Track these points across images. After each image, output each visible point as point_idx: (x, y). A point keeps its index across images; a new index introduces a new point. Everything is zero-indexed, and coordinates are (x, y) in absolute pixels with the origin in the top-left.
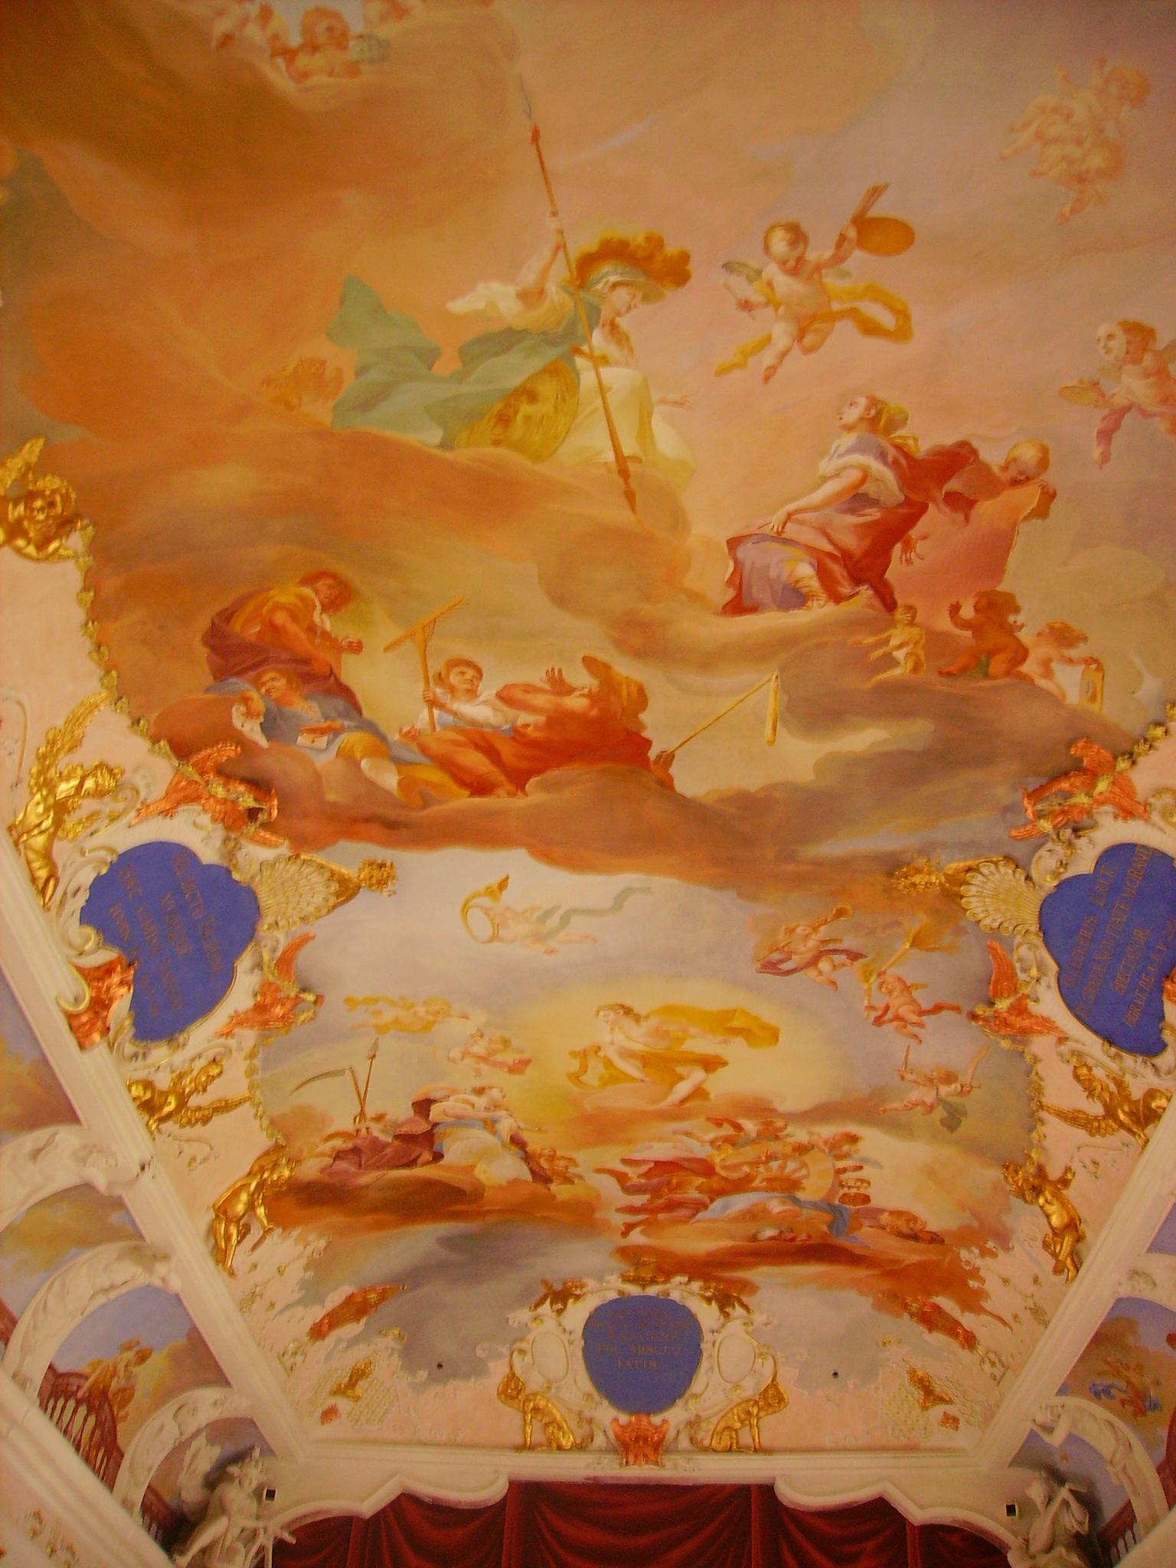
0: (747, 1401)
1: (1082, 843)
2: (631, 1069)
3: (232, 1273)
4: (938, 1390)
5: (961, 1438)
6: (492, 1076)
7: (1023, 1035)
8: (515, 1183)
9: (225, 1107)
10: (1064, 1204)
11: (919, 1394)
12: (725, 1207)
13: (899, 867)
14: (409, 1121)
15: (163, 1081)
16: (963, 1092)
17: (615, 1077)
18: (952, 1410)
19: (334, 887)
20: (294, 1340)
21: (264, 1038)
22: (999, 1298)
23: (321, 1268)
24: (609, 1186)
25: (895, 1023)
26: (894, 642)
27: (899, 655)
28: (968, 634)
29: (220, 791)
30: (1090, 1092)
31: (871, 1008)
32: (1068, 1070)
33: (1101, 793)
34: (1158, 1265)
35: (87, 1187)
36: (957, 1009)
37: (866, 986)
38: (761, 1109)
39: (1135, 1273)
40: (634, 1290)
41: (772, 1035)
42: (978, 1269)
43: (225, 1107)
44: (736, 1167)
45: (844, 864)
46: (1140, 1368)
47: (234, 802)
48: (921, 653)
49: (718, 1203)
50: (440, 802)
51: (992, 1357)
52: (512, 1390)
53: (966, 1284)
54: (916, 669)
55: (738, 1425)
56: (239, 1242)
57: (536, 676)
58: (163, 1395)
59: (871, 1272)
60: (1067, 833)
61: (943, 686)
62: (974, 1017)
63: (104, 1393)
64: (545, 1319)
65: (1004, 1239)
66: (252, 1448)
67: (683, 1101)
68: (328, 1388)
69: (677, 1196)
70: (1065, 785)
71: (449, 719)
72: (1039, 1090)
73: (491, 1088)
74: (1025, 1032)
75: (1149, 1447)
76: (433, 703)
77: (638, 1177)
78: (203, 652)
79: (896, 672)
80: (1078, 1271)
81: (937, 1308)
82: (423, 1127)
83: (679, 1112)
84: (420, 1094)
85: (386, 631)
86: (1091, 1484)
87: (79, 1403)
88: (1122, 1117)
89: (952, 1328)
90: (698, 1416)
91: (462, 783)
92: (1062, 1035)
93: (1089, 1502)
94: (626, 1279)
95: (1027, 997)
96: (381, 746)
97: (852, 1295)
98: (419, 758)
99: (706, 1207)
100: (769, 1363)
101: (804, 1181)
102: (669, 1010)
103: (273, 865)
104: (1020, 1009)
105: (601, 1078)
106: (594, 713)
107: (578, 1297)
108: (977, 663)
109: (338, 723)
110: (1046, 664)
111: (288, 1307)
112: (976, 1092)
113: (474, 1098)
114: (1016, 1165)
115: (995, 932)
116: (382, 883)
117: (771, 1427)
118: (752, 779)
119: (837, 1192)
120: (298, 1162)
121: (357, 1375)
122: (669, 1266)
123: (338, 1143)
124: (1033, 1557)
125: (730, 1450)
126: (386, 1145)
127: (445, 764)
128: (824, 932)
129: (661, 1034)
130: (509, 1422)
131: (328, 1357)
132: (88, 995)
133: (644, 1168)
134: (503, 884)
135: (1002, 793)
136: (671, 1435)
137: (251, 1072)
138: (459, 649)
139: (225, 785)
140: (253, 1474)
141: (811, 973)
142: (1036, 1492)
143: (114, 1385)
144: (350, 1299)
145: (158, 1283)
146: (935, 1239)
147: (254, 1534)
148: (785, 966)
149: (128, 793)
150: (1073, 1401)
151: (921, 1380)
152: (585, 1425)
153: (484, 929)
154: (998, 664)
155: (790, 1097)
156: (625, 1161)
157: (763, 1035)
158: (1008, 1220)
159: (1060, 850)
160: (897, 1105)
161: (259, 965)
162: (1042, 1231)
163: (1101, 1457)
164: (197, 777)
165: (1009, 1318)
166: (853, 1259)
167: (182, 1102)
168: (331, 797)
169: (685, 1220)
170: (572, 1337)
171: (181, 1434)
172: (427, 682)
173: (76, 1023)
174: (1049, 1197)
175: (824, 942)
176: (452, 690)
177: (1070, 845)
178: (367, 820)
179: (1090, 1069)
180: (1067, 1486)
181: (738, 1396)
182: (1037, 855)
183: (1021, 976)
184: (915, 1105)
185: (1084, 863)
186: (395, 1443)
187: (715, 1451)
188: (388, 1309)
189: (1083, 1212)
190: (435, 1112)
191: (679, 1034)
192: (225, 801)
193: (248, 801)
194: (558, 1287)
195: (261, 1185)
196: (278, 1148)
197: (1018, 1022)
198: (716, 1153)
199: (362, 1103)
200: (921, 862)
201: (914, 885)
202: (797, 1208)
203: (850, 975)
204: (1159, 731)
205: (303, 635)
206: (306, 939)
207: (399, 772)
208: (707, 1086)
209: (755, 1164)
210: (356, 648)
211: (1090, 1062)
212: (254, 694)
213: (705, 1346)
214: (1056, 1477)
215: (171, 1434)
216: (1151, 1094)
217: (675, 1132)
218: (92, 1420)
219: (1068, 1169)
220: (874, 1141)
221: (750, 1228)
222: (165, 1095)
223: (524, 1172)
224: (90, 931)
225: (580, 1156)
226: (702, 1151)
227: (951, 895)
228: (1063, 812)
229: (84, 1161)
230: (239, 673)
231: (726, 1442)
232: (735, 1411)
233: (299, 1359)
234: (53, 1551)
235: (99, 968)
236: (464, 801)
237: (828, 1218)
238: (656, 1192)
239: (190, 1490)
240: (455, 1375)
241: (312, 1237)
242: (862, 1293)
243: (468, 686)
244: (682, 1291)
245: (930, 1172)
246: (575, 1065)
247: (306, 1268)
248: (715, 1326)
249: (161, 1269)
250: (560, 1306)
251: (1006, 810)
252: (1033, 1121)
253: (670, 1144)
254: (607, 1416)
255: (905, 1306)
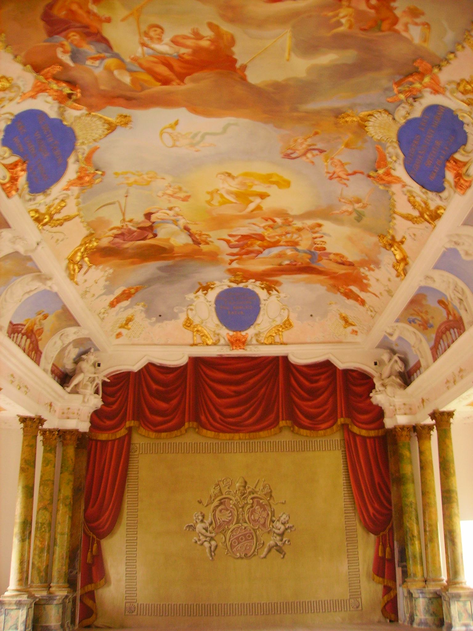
0: (278, 326)
1: (416, 104)
2: (231, 198)
3: (77, 284)
4: (350, 321)
5: (358, 338)
6: (176, 203)
7: (388, 184)
8: (186, 245)
9: (68, 219)
10: (401, 250)
11: (343, 323)
12: (269, 253)
13: (340, 114)
14: (143, 222)
15: (43, 210)
16: (364, 207)
17: (225, 202)
18: (355, 328)
19: (106, 126)
20: (103, 308)
21: (82, 190)
22: (375, 287)
23: (112, 281)
24: (223, 246)
25: (337, 179)
26: (341, 15)
27: (343, 21)
28: (373, 11)
29: (55, 86)
30: (414, 206)
31: (328, 173)
32: (405, 198)
33: (425, 83)
34: (437, 275)
35: (17, 253)
36: (362, 173)
37: (326, 164)
38: (283, 214)
39: (427, 277)
40: (234, 285)
41: (287, 184)
42: (367, 276)
43: (68, 219)
44: (274, 237)
45: (318, 113)
46: (427, 313)
47: (61, 91)
48: (352, 20)
49: (266, 251)
50: (150, 88)
51: (372, 309)
52: (188, 324)
53: (362, 281)
54: (350, 27)
55: (274, 335)
56: (79, 271)
57: (187, 32)
58: (54, 331)
59: (326, 277)
60: (411, 100)
61: (361, 35)
62: (369, 176)
63: (32, 331)
64: (200, 297)
65: (377, 264)
66: (90, 349)
67: (252, 211)
68: (118, 325)
69: (250, 249)
70: (411, 79)
71: (151, 51)
72: (394, 206)
73: (175, 207)
74: (389, 183)
75: (428, 340)
76: (143, 45)
77: (236, 241)
78: (42, 24)
79: (341, 29)
80: (405, 276)
81: (351, 291)
82: (148, 224)
83: (251, 216)
84: (147, 210)
85: (121, 12)
86: (405, 354)
87: (23, 335)
88: (426, 217)
89: (356, 298)
90: (259, 332)
91: (158, 80)
92: (403, 184)
93: (405, 361)
94: (231, 281)
95: (391, 168)
96: (122, 65)
97: (318, 286)
98: (139, 69)
99: (261, 252)
100: (286, 312)
101: (300, 242)
102: (246, 174)
103: (79, 118)
104: (388, 174)
105: (219, 202)
106: (213, 48)
107: (212, 288)
108: (377, 25)
109: (103, 55)
110: (406, 25)
111: (101, 295)
112: (369, 207)
113: (168, 212)
114: (383, 235)
115: (379, 142)
116: (126, 124)
117: (286, 335)
118: (280, 76)
119: (313, 246)
120: (100, 239)
121: (129, 320)
122: (247, 276)
123: (115, 232)
124: (383, 380)
125: (271, 344)
126: (134, 232)
127: (150, 72)
128: (309, 141)
129: (243, 184)
130: (188, 336)
131: (117, 314)
132: (8, 175)
133: (237, 238)
134: (176, 123)
135: (385, 83)
136: (249, 338)
137: (78, 204)
138: (154, 20)
139: (57, 84)
140: (92, 358)
141: (304, 158)
142: (385, 357)
143: (36, 328)
144: (124, 293)
145: (48, 289)
146: (351, 264)
147: (94, 380)
148: (293, 156)
149: (15, 89)
150: (400, 325)
151: (344, 317)
152: (216, 336)
153: (170, 142)
154: (385, 25)
155: (295, 210)
156: (230, 236)
157: (284, 184)
158: (380, 257)
159: (407, 107)
160: (337, 212)
161: (77, 161)
162: (392, 260)
163: (409, 344)
164: (44, 81)
165: (378, 294)
166: (319, 272)
167: (51, 218)
168: (102, 87)
169: (253, 258)
170: (210, 303)
171: (64, 344)
172: (140, 36)
173: (5, 187)
174: (396, 248)
175: (310, 145)
176: (151, 38)
177: (411, 105)
178: (118, 97)
179: (414, 197)
180: (397, 355)
181: (275, 324)
182: (397, 109)
183: (389, 160)
184: (345, 212)
185: (417, 112)
186: (144, 345)
187: (266, 344)
188: (139, 295)
189: (409, 253)
190: (153, 218)
191: (250, 184)
192: (57, 91)
193: (67, 90)
194: (204, 285)
195: (86, 249)
196: (91, 234)
197: (387, 178)
198: (265, 231)
199: (124, 214)
200: (349, 112)
201: (347, 122)
202: (297, 252)
203: (319, 159)
204: (452, 56)
205: (85, 15)
206: (97, 149)
207: (131, 76)
208: (262, 205)
209: (280, 236)
210: (109, 20)
211: (415, 195)
212: (65, 43)
213: (261, 306)
214: (393, 352)
215: (59, 345)
216: (438, 208)
217: (250, 223)
218: (29, 341)
219: (404, 237)
220: (328, 226)
221: (279, 261)
222: (44, 215)
223: (189, 240)
224: (6, 149)
225: (211, 233)
226: (260, 231)
227: (362, 126)
228: (410, 91)
229: (14, 243)
230: (58, 33)
231: (270, 341)
232: (273, 329)
233: (106, 315)
234: (20, 388)
235: (11, 164)
236: (158, 88)
237: (309, 256)
238: (242, 247)
239: (69, 365)
240: (166, 319)
241: (107, 268)
242: (323, 285)
243: (158, 36)
244: (253, 285)
245: (350, 239)
246: (208, 197)
247: (106, 281)
248: (265, 298)
249: (49, 283)
250: (205, 292)
251: (387, 89)
252: (391, 218)
253: (247, 228)
254: (225, 333)
255: (339, 290)
